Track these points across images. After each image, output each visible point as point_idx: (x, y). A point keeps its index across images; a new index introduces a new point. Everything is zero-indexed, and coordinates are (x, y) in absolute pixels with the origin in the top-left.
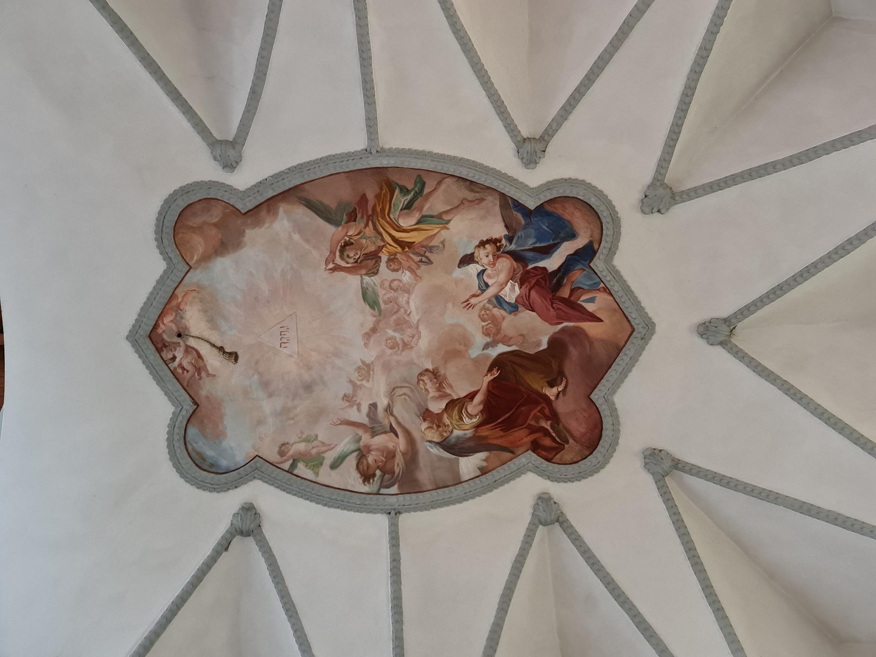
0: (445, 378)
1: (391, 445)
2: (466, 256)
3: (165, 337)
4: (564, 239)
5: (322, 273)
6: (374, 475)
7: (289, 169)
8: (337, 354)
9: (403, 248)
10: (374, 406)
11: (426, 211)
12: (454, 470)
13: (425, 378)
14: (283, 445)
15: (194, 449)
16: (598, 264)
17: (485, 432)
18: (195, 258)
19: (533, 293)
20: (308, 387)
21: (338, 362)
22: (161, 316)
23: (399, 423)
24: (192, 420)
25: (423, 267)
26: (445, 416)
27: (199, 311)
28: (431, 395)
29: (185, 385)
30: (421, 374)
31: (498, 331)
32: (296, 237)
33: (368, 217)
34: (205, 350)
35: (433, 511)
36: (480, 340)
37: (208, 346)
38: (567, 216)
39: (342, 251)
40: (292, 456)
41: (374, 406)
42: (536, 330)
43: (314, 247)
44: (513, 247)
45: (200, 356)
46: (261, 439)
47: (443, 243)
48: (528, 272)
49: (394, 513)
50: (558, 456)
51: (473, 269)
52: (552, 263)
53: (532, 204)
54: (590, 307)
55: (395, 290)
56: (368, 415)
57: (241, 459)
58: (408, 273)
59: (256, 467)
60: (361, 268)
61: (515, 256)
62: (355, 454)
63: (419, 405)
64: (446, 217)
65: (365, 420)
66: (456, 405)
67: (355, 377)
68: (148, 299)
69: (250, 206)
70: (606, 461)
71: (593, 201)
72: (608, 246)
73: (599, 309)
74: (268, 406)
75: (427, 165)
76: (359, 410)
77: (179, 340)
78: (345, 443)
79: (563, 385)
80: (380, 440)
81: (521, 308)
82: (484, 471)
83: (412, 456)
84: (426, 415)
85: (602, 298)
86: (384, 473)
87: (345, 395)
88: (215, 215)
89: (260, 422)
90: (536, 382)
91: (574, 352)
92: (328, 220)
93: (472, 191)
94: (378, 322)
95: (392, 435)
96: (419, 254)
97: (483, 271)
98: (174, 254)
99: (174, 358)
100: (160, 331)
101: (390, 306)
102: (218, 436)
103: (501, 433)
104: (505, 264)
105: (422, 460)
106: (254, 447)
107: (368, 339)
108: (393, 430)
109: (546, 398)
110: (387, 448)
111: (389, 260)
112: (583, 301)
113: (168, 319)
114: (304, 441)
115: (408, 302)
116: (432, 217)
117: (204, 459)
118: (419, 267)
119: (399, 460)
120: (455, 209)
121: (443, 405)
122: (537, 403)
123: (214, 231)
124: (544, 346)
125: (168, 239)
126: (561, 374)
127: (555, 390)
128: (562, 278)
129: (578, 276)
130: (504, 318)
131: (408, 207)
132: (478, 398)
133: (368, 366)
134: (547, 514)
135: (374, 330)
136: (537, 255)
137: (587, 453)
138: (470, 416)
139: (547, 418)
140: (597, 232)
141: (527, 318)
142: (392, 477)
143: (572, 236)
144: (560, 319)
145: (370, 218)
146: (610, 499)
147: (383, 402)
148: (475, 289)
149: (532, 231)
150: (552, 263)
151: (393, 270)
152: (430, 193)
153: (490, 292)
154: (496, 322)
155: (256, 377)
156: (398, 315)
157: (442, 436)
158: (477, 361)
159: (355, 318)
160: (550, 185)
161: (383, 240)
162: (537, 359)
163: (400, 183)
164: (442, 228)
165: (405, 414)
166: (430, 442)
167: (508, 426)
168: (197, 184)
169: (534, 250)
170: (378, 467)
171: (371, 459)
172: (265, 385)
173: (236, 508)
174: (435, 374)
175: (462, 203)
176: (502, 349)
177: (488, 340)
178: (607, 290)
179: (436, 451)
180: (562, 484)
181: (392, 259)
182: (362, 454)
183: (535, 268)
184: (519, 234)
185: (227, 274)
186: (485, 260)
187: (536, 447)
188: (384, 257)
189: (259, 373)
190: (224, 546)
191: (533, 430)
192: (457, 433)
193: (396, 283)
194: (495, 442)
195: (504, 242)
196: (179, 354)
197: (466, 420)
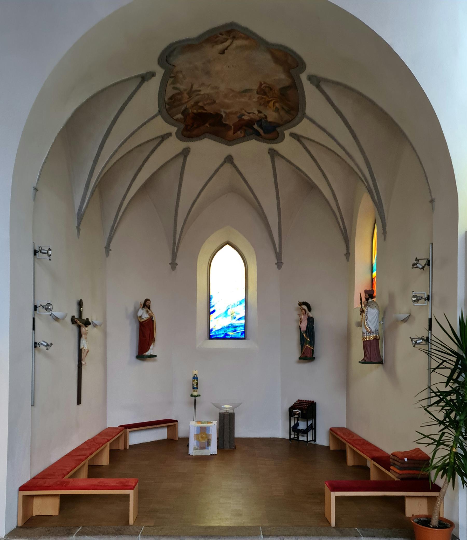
10: (200, 91)
34: (226, 44)
36: (228, 111)
44: (263, 120)
49: (160, 112)
51: (256, 112)
52: (256, 126)
53: (278, 129)
54: (239, 132)
75: (297, 119)
77: (231, 36)
78: (182, 87)
80: (186, 96)
82: (177, 120)
85: (242, 135)
99: (222, 35)
104: (257, 118)
108: (190, 97)
109: (206, 123)
111: (263, 98)
124: (224, 123)
134: (163, 138)
135: (233, 91)
146: (174, 146)
150: (256, 126)
159: (238, 86)
176: (224, 115)
179: (183, 108)
182: (181, 93)
188: (265, 97)
196: (224, 37)
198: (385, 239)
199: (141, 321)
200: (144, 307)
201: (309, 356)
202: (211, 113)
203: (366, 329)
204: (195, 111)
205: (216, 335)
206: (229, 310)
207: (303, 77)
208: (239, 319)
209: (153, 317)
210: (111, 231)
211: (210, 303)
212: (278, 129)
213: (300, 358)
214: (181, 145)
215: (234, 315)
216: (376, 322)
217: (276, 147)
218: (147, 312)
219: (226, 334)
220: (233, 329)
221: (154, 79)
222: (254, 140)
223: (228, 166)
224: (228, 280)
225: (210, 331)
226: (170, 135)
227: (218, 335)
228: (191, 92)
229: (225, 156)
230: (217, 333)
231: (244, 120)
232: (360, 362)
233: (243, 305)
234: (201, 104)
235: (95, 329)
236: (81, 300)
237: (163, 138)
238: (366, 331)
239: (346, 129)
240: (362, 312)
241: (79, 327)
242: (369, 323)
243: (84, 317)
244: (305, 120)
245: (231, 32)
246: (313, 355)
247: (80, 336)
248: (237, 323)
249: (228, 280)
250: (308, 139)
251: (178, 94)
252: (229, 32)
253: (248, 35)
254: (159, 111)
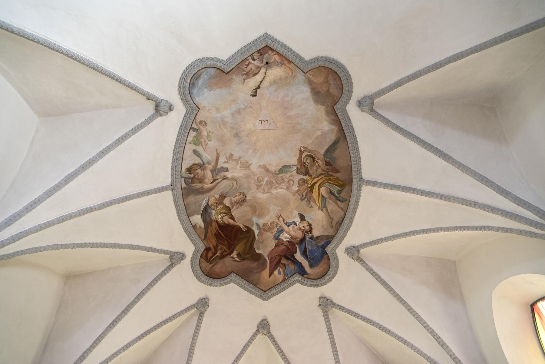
0: (241, 205)
1: (206, 180)
2: (304, 217)
3: (266, 55)
4: (309, 262)
5: (299, 144)
6: (191, 174)
7: (355, 136)
8: (255, 151)
9: (310, 187)
11: (328, 200)
12: (195, 213)
13: (242, 196)
14: (206, 123)
15: (202, 73)
16: (297, 277)
17: (214, 225)
18: (311, 77)
19: (284, 247)
20: (237, 135)
21: (251, 151)
22: (278, 54)
23: (218, 183)
24: (219, 71)
25: (300, 197)
26: (222, 206)
27: (281, 76)
28: (233, 199)
29: (238, 66)
30: (244, 194)
31: (265, 230)
32: (319, 133)
33: (327, 172)
34: (259, 77)
35: (174, 206)
36: (261, 222)
37: (261, 80)
38: (320, 264)
39: (310, 156)
40: (199, 128)
41: (227, 170)
42: (266, 247)
43: (313, 141)
44: (307, 239)
45: (255, 75)
46: (209, 110)
47: (312, 207)
48: (294, 245)
49: (172, 188)
50: (203, 260)
51: (297, 220)
52: (298, 256)
54: (276, 272)
55: (288, 182)
56: (222, 167)
57: (197, 100)
58: (297, 189)
59: (192, 109)
60: (301, 165)
61: (303, 240)
62: (202, 163)
63: (227, 193)
64: (324, 209)
65: (219, 166)
66: (228, 211)
67: (243, 160)
68: (288, 48)
69: (337, 112)
70: (200, 281)
71: (327, 277)
72: (305, 282)
73: (275, 276)
74: (227, 113)
75: (351, 206)
76: (225, 162)
77: (265, 61)
78: (207, 156)
79: (238, 260)
80: (209, 174)
81: (277, 241)
82: (194, 227)
83: (201, 192)
84: (223, 197)
85: (281, 277)
86: (192, 179)
87: (232, 155)
88: (334, 91)
89: (218, 109)
90: (239, 247)
91: (255, 265)
92: (327, 151)
93: (337, 223)
94: (272, 173)
95: (212, 181)
96: (306, 196)
97: (296, 225)
98: (313, 66)
99: (254, 60)
100: (270, 52)
101: (280, 179)
102: (210, 86)
103: (214, 233)
104: (300, 235)
105: (199, 197)
106: (204, 107)
107: (262, 168)
108: (214, 181)
109: (232, 252)
110: (205, 178)
111: (304, 180)
112: (279, 270)
113: (276, 57)
114: (208, 134)
115: (281, 188)
116: (325, 203)
117: (197, 79)
118: (300, 195)
119: (199, 185)
120: (328, 214)
121: (228, 204)
122: (229, 249)
123: (325, 89)
124: (257, 251)
125: (322, 64)
126: (244, 259)
127: (235, 256)
128: (291, 260)
129: (292, 267)
130: (272, 233)
131: (331, 192)
132: (231, 221)
133: (248, 167)
134: (175, 258)
135: (267, 170)
136: (303, 250)
137: (206, 273)
138: (222, 218)
139: (222, 254)
140: (312, 277)
141: (272, 244)
142: (190, 183)
143: (311, 266)
144: (271, 259)
145: (327, 173)
146: (185, 285)
147: (229, 175)
148: (287, 220)
149: (315, 248)
150: (298, 256)
151: (299, 182)
152: (337, 204)
153: (285, 227)
154: (270, 229)
155: (243, 106)
156: (275, 183)
157: (212, 205)
158: (250, 220)
159: (274, 161)
160: (336, 259)
161: (315, 178)
162: (251, 247)
163: (344, 191)
164: (319, 207)
165: (223, 186)
166: (209, 200)
167: (218, 236)
168: (351, 84)
169: (305, 248)
170: (195, 175)
171: (199, 171)
172: (239, 112)
173: (170, 101)
174: (244, 200)
175: (331, 218)
176: (256, 232)
177: (261, 226)
178: (284, 280)
179: (204, 203)
180: (190, 263)
181: (304, 181)
182: (202, 166)
183: (296, 248)
184: (314, 242)
185: (301, 94)
186: (301, 226)
187: (208, 249)
188: (306, 178)
189: (245, 108)
190: (149, 97)
191: (216, 248)
192: (214, 212)
193: (292, 183)
194: (209, 231)
195: (310, 235)
196: (256, 63)
197: (220, 216)
217: (330, 289)
223: (262, 338)
234: (227, 202)
239: (400, 305)
244: (366, 190)
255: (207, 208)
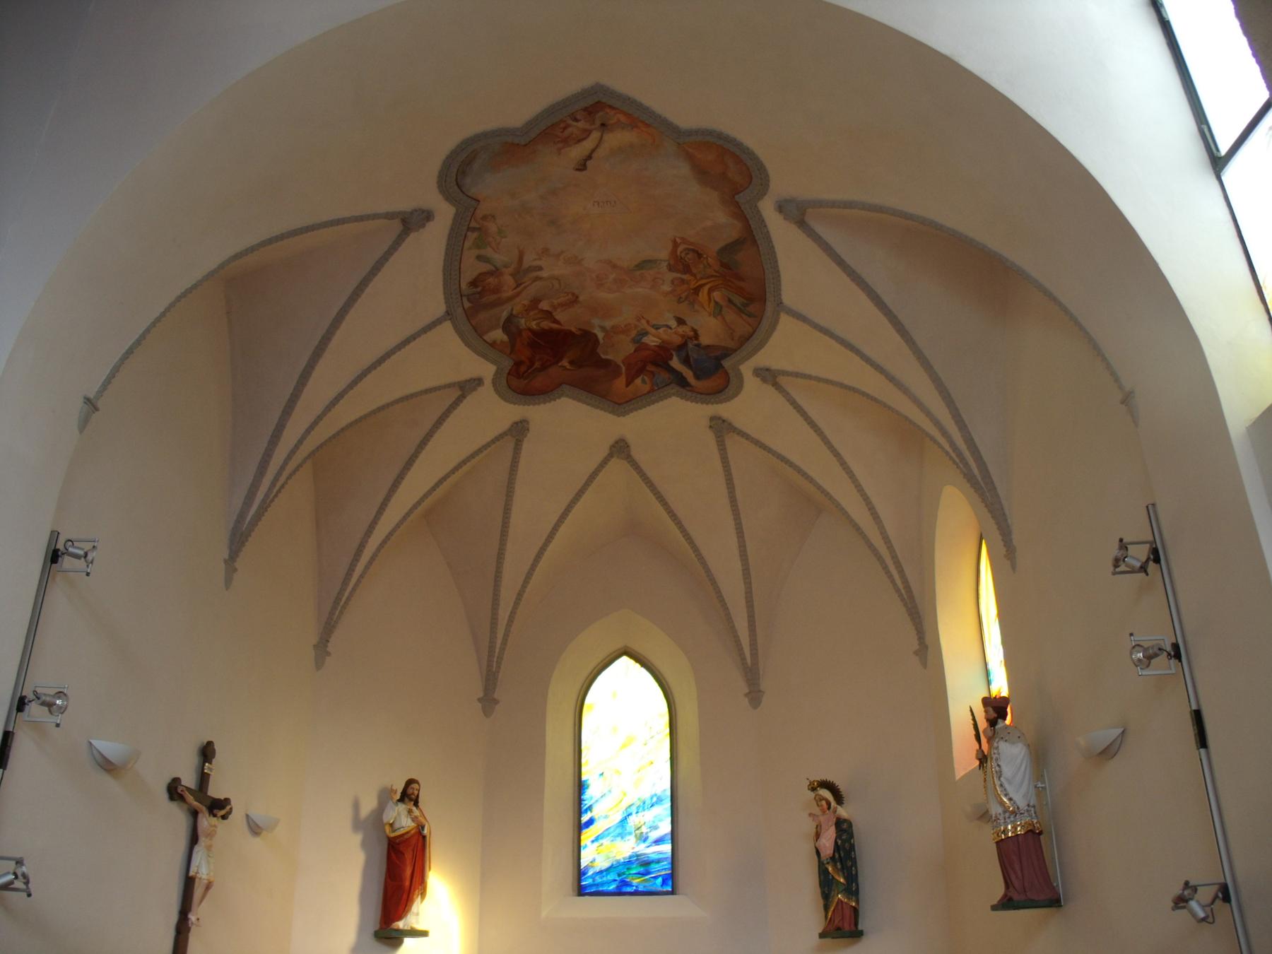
10: (540, 268)
32: (709, 223)
34: (588, 145)
36: (608, 324)
41: (540, 268)
44: (690, 345)
45: (579, 141)
49: (449, 314)
51: (673, 324)
52: (675, 363)
53: (727, 363)
54: (638, 381)
65: (526, 264)
75: (765, 324)
77: (598, 123)
78: (499, 258)
80: (508, 280)
82: (493, 344)
85: (647, 388)
99: (576, 120)
104: (677, 340)
108: (518, 286)
109: (561, 359)
111: (683, 281)
113: (622, 118)
119: (493, 297)
129: (663, 376)
131: (730, 301)
134: (467, 387)
135: (614, 266)
138: (538, 324)
141: (631, 348)
143: (697, 377)
146: (490, 412)
147: (544, 274)
150: (675, 363)
153: (653, 331)
160: (740, 377)
171: (491, 280)
176: (600, 335)
179: (505, 315)
182: (496, 272)
187: (518, 364)
188: (685, 277)
196: (581, 125)
198: (1014, 567)
199: (393, 835)
200: (401, 800)
201: (847, 928)
202: (571, 332)
203: (1002, 803)
204: (534, 325)
205: (597, 885)
206: (630, 819)
207: (767, 208)
208: (658, 841)
209: (423, 827)
210: (334, 608)
211: (580, 801)
212: (727, 363)
213: (822, 935)
214: (507, 412)
215: (644, 830)
216: (1026, 782)
217: (724, 409)
218: (410, 812)
219: (624, 883)
220: (641, 869)
221: (430, 225)
222: (674, 398)
223: (617, 465)
224: (625, 732)
225: (580, 873)
226: (478, 382)
227: (602, 884)
228: (520, 273)
229: (611, 441)
230: (598, 880)
231: (646, 347)
232: (994, 908)
233: (668, 804)
234: (544, 305)
235: (257, 840)
236: (210, 744)
237: (467, 387)
238: (1000, 810)
240: (983, 759)
241: (195, 814)
242: (1006, 785)
243: (215, 791)
244: (785, 320)
245: (596, 110)
246: (856, 924)
247: (194, 839)
248: (651, 851)
249: (625, 732)
250: (796, 375)
251: (491, 273)
252: (595, 112)
253: (638, 118)
254: (448, 313)
255: (510, 319)
